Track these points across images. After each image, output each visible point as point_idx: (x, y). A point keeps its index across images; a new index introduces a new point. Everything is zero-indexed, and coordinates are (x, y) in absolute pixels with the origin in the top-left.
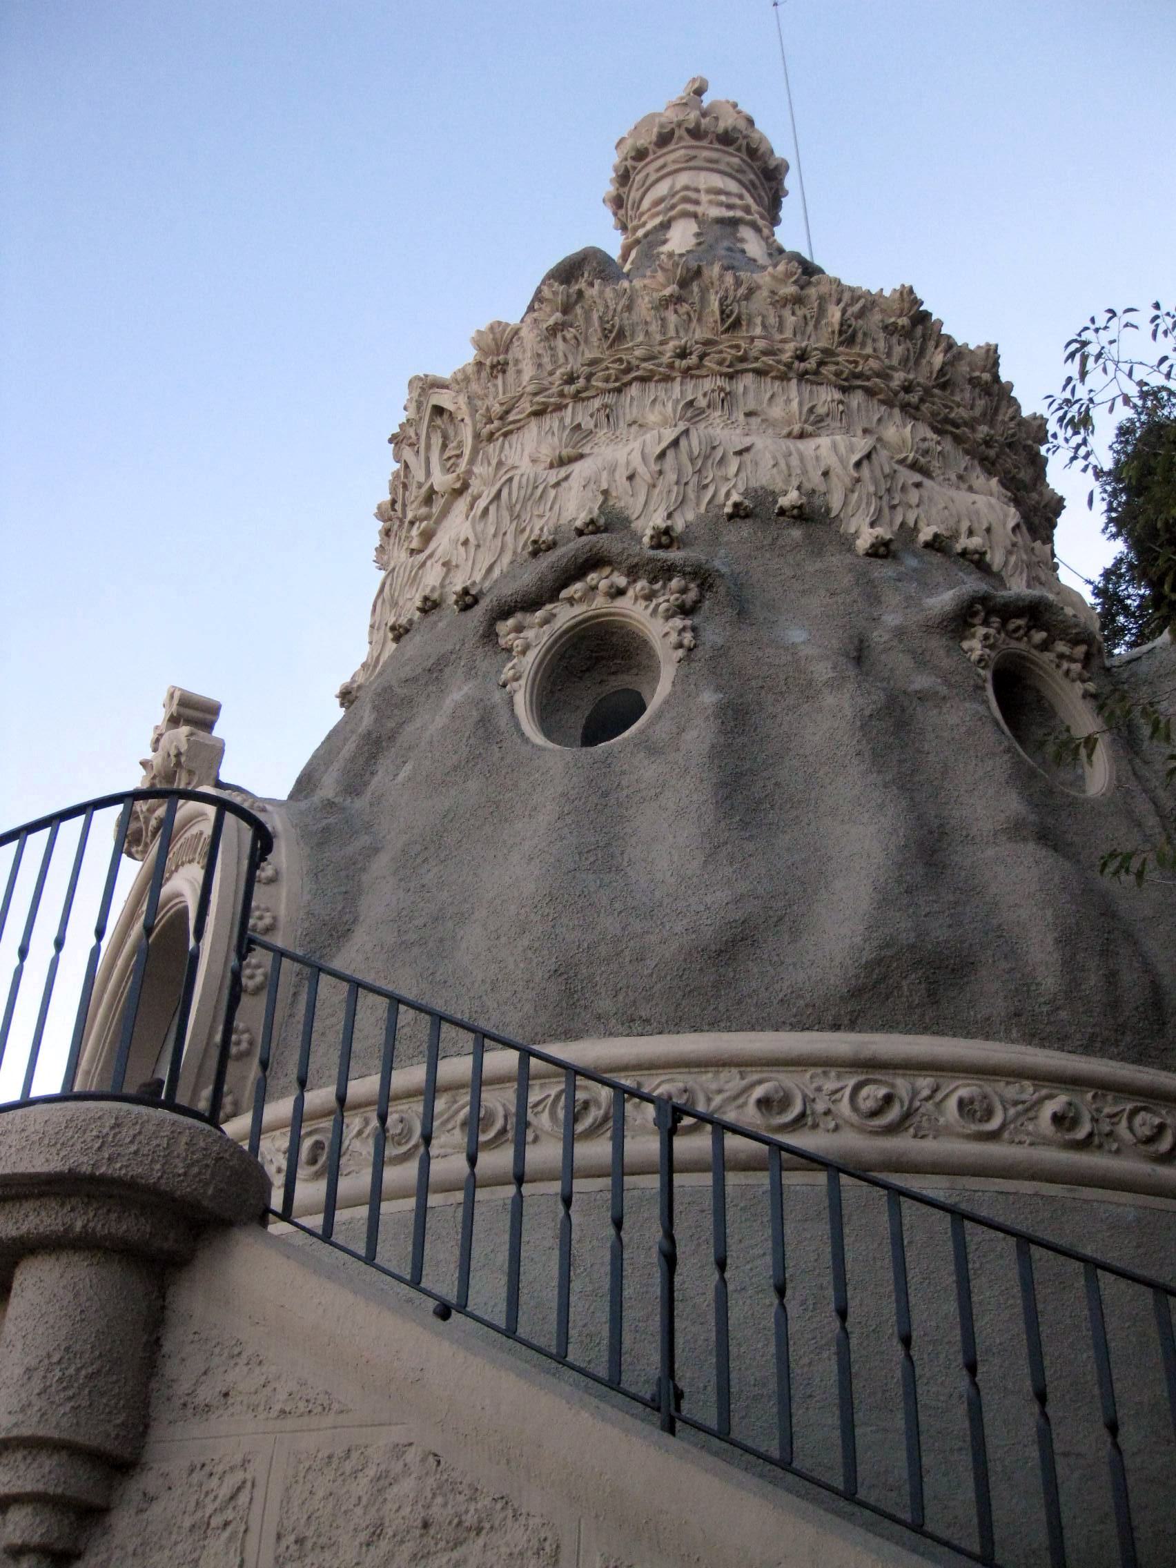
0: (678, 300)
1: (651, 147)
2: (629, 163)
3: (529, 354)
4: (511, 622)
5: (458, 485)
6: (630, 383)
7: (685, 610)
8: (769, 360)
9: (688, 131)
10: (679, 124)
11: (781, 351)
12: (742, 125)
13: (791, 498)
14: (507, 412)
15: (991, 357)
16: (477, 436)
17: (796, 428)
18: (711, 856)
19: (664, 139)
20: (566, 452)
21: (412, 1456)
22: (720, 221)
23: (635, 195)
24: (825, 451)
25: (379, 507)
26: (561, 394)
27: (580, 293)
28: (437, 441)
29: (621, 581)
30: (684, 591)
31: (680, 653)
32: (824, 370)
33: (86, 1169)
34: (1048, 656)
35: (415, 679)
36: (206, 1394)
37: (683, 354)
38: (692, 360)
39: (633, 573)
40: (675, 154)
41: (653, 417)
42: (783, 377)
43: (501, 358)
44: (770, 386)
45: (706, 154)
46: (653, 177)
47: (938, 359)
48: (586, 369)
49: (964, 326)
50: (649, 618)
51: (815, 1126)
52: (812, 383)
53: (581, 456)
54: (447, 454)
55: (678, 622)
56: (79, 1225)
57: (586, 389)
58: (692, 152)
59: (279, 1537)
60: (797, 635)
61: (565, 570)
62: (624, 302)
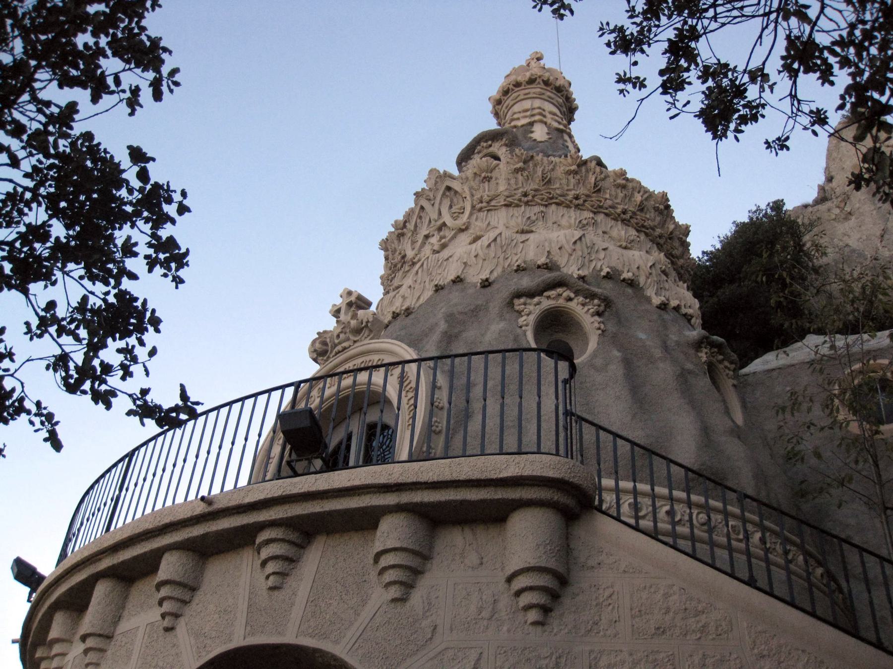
0: (575, 173)
1: (524, 83)
2: (511, 87)
3: (503, 177)
4: (522, 300)
5: (464, 227)
6: (551, 204)
7: (599, 314)
8: (562, 199)
9: (543, 81)
10: (540, 77)
11: (567, 195)
12: (566, 85)
13: (627, 275)
14: (491, 200)
15: (686, 231)
16: (473, 207)
17: (624, 244)
18: (634, 416)
19: (531, 81)
20: (525, 228)
21: (675, 588)
22: (558, 130)
23: (509, 102)
24: (562, 238)
25: (396, 222)
26: (520, 200)
27: (532, 157)
28: (446, 202)
29: (572, 295)
30: (599, 306)
31: (600, 332)
32: (632, 221)
33: (566, 478)
34: (721, 366)
35: (466, 314)
36: (591, 562)
37: (577, 198)
38: (581, 201)
39: (577, 293)
40: (535, 90)
41: (564, 222)
42: (568, 207)
43: (489, 175)
44: (562, 210)
45: (549, 94)
46: (522, 97)
47: (672, 227)
48: (533, 193)
49: (681, 216)
50: (583, 313)
51: (684, 525)
52: (627, 225)
53: (532, 232)
54: (453, 210)
55: (597, 318)
56: (556, 498)
57: (531, 201)
58: (543, 91)
59: (631, 609)
60: (642, 336)
61: (549, 284)
62: (551, 167)
